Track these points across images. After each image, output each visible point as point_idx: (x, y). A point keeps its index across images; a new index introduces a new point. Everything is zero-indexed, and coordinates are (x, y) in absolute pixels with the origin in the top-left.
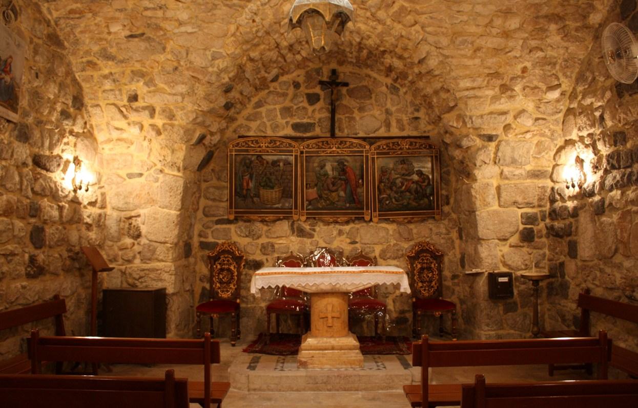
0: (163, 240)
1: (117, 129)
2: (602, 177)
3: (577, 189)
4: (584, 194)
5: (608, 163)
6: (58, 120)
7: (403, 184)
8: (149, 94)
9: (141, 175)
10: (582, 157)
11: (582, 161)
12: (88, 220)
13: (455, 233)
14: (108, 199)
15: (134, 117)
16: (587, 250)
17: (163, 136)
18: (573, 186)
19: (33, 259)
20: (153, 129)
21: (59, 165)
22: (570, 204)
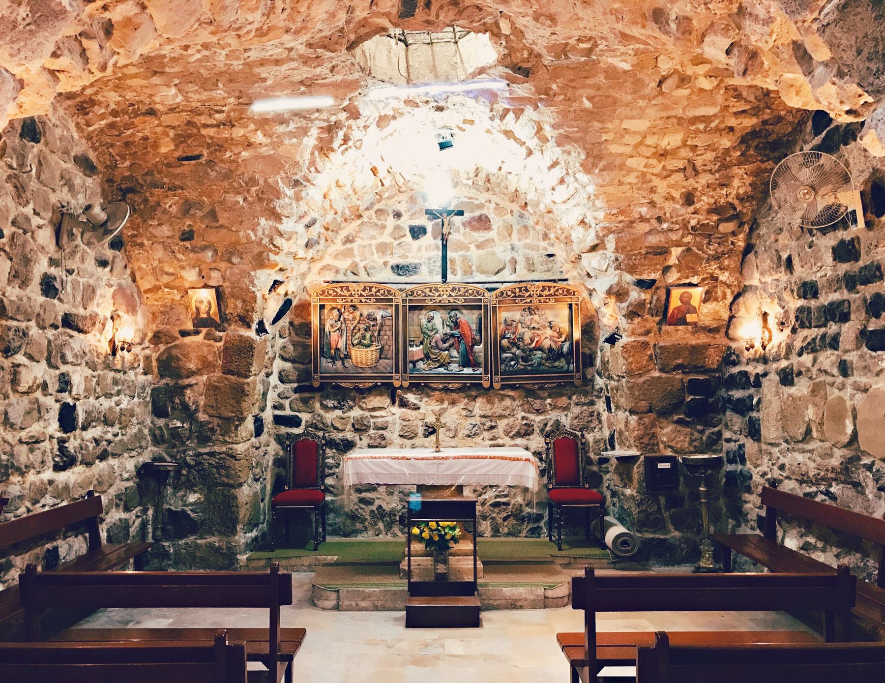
7: (532, 340)
13: (602, 404)
16: (773, 429)
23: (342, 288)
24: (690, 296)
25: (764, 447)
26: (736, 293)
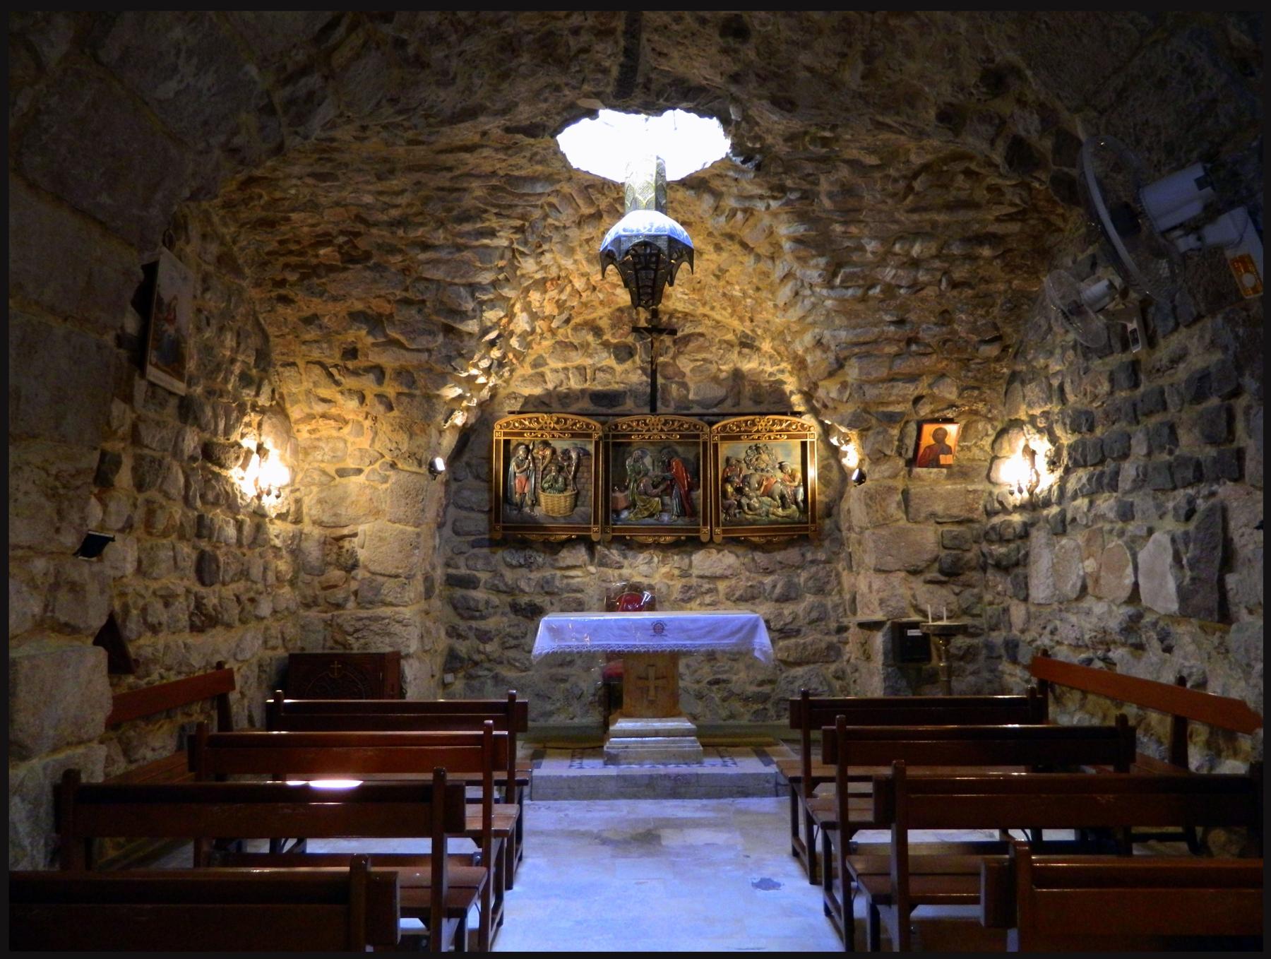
0: (393, 572)
1: (324, 400)
2: (1061, 478)
3: (1026, 495)
4: (1034, 505)
5: (1070, 458)
6: (235, 388)
8: (376, 349)
9: (359, 471)
10: (1033, 446)
11: (1033, 453)
12: (278, 542)
14: (305, 510)
15: (349, 382)
16: (1042, 588)
17: (395, 413)
18: (1020, 491)
19: (199, 605)
20: (381, 403)
21: (238, 458)
22: (1017, 518)
23: (531, 419)
24: (945, 433)
25: (1033, 609)
26: (999, 428)
